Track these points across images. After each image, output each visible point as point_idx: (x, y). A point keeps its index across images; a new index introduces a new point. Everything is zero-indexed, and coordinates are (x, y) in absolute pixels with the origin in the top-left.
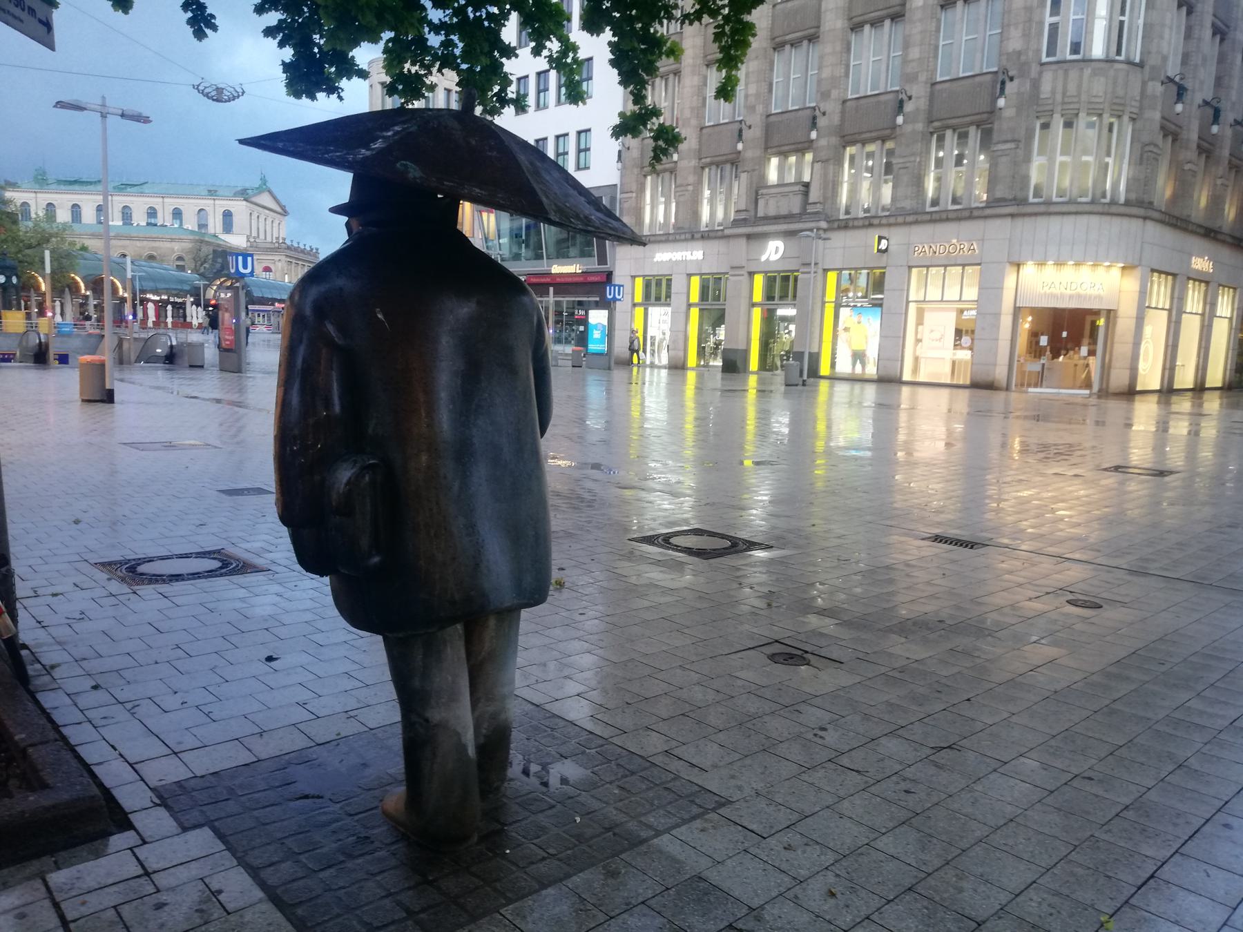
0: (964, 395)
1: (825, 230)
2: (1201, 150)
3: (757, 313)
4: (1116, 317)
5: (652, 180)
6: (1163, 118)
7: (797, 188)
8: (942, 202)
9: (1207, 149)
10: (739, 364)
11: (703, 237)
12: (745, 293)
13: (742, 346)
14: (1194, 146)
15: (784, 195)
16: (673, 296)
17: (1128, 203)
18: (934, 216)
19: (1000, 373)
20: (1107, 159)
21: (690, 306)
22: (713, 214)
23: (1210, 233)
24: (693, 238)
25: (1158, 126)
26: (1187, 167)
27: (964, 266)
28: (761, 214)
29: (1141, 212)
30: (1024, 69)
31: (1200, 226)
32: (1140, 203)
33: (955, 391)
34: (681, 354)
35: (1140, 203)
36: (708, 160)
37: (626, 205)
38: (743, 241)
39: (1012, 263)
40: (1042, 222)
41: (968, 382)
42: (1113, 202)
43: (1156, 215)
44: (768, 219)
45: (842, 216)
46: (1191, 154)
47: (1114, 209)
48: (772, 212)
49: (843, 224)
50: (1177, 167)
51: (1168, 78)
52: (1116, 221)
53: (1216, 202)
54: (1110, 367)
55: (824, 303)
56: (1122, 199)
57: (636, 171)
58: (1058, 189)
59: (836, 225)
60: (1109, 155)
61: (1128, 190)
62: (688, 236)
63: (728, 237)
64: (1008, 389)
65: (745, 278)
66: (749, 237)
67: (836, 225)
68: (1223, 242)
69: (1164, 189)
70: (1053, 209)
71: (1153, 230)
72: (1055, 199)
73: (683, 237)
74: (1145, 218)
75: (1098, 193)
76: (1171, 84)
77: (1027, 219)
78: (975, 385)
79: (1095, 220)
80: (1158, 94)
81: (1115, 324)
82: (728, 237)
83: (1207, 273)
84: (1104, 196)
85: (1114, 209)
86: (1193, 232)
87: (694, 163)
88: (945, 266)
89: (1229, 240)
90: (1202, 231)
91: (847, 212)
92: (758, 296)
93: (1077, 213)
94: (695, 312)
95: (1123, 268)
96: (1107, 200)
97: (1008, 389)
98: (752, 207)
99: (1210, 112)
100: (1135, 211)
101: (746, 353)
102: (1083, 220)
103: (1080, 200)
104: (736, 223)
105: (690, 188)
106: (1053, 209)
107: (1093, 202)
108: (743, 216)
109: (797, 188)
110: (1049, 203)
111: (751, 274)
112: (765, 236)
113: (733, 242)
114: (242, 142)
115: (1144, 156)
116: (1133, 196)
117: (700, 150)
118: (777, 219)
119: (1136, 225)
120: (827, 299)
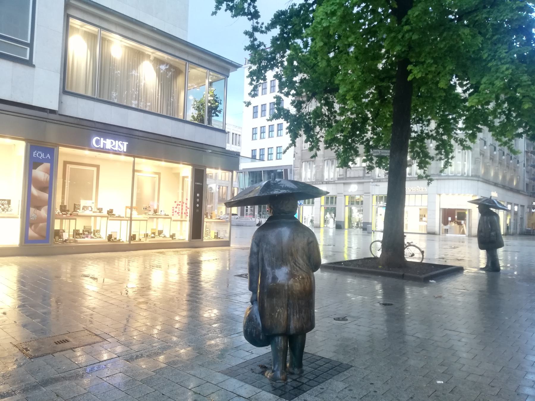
0: (425, 236)
1: (372, 182)
2: (491, 159)
3: (347, 208)
4: (472, 211)
5: (305, 164)
6: (480, 150)
7: (361, 168)
8: (412, 174)
9: (492, 158)
10: (342, 226)
11: (326, 183)
12: (343, 202)
13: (343, 220)
14: (489, 158)
15: (356, 170)
16: (315, 203)
17: (472, 176)
18: (411, 179)
19: (437, 230)
20: (465, 163)
21: (321, 206)
22: (329, 176)
23: (496, 185)
24: (323, 183)
25: (479, 152)
26: (488, 164)
27: (422, 195)
28: (348, 176)
29: (477, 179)
30: (415, 121)
31: (493, 182)
32: (476, 176)
33: (421, 235)
34: (319, 223)
35: (476, 176)
36: (327, 158)
37: (296, 172)
38: (342, 185)
39: (438, 194)
40: (447, 181)
41: (425, 232)
42: (468, 176)
43: (481, 180)
44: (350, 178)
45: (377, 178)
46: (488, 160)
47: (469, 178)
48: (352, 176)
49: (379, 180)
50: (485, 165)
51: (481, 138)
52: (470, 181)
53: (496, 174)
54: (471, 228)
55: (372, 206)
56: (470, 175)
57: (300, 161)
58: (451, 172)
59: (376, 181)
60: (465, 161)
61: (472, 172)
62: (321, 183)
63: (337, 183)
64: (439, 234)
65: (343, 197)
66: (344, 184)
67: (376, 181)
68: (500, 187)
69: (482, 171)
70: (450, 178)
71: (481, 184)
72: (450, 175)
73: (319, 183)
74: (478, 181)
75: (463, 173)
76: (492, 146)
77: (442, 181)
78: (429, 233)
79: (463, 181)
80: (464, 132)
81: (471, 214)
82: (337, 183)
83: (496, 197)
84: (465, 174)
85: (469, 178)
86: (491, 184)
87: (322, 159)
88: (415, 195)
89: (501, 186)
90: (494, 184)
91: (378, 176)
92: (347, 204)
93: (458, 179)
94: (323, 208)
95: (473, 196)
96: (466, 175)
97: (439, 234)
98: (345, 174)
99: (493, 148)
100: (475, 178)
101: (344, 222)
102: (460, 181)
103: (458, 175)
104: (339, 179)
105: (321, 167)
106: (450, 178)
107: (462, 176)
108: (342, 177)
109: (361, 168)
110: (449, 176)
111: (345, 196)
112: (350, 183)
113: (338, 185)
114: (468, 202)
115: (475, 161)
116: (474, 174)
117: (324, 155)
118: (354, 178)
119: (475, 183)
120: (373, 205)
